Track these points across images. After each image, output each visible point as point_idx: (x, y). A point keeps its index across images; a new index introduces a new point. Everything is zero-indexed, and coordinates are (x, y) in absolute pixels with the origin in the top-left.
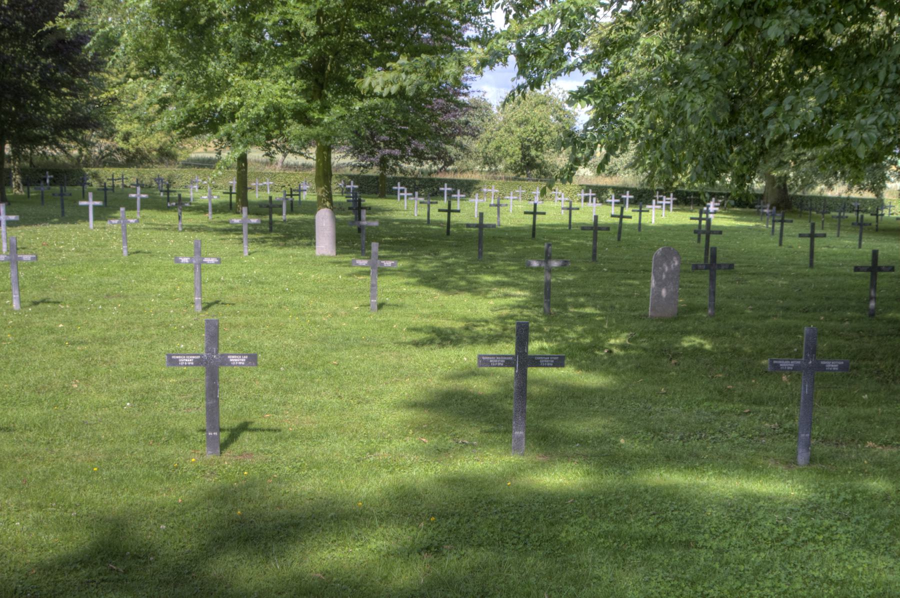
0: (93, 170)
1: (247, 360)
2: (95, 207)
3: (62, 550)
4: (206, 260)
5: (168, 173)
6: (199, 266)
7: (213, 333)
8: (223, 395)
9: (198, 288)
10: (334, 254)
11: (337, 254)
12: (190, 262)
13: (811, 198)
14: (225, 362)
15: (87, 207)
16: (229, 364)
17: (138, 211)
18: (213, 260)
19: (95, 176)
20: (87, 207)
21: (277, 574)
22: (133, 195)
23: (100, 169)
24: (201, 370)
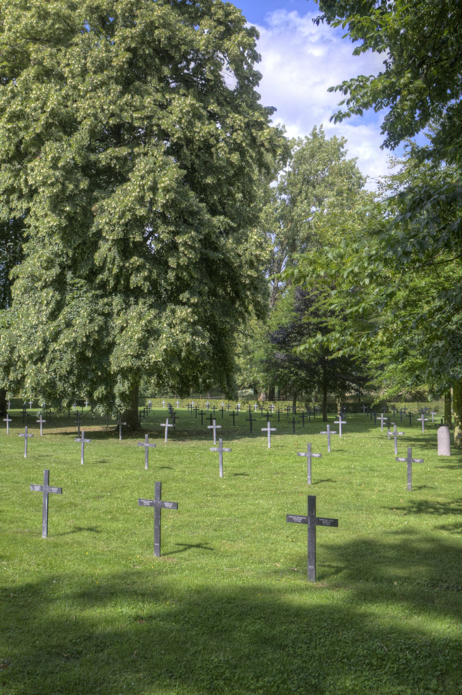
0: (392, 404)
1: (173, 506)
2: (342, 424)
3: (34, 577)
4: (313, 455)
5: (434, 405)
6: (410, 460)
7: (159, 492)
8: (163, 523)
9: (309, 471)
10: (449, 455)
11: (451, 455)
12: (305, 456)
13: (18, 399)
14: (163, 506)
15: (338, 424)
16: (165, 507)
17: (382, 427)
18: (317, 455)
19: (394, 408)
20: (338, 424)
21: (191, 597)
22: (379, 418)
23: (396, 403)
24: (152, 509)
